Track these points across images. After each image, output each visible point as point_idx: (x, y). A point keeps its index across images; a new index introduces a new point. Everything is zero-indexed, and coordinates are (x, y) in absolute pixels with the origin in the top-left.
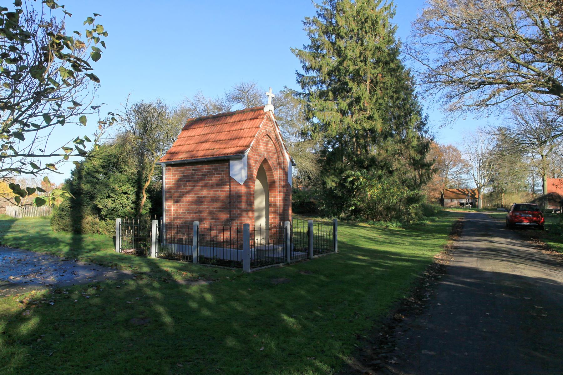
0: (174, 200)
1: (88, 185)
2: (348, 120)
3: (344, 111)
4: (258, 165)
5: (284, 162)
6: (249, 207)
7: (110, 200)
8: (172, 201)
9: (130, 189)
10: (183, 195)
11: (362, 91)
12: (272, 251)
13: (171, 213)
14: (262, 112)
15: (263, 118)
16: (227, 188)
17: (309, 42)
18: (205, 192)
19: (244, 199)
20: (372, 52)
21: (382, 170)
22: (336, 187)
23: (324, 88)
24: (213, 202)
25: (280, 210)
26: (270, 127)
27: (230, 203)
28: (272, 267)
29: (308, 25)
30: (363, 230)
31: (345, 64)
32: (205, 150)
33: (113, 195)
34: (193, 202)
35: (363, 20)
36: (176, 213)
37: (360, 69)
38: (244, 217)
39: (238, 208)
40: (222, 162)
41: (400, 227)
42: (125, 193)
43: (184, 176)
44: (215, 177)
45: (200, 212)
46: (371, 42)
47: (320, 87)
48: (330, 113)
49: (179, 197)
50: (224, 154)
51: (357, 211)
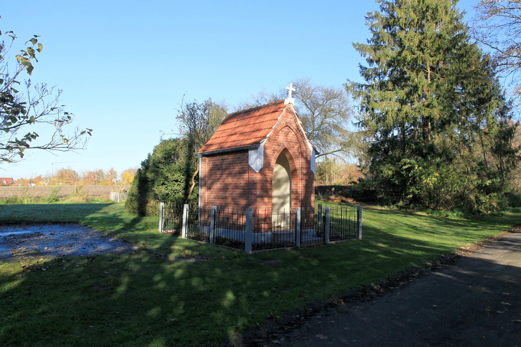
1: (153, 174)
2: (407, 108)
3: (402, 100)
4: (277, 155)
5: (306, 151)
6: (265, 193)
7: (164, 186)
9: (181, 177)
10: (214, 182)
11: (422, 80)
12: (288, 236)
13: (205, 198)
14: (282, 105)
15: (282, 111)
16: (246, 176)
17: (371, 36)
18: (229, 180)
19: (259, 186)
20: (432, 40)
21: (441, 158)
22: (393, 175)
23: (387, 78)
26: (291, 118)
27: (248, 189)
28: (277, 250)
29: (371, 20)
30: (416, 219)
31: (403, 54)
32: (232, 142)
33: (166, 182)
34: (222, 189)
35: (424, 9)
36: (209, 198)
37: (417, 57)
40: (241, 152)
41: (461, 216)
42: (177, 181)
43: (216, 165)
44: (238, 166)
45: (225, 198)
46: (433, 29)
47: (381, 79)
48: (389, 104)
49: (211, 184)
50: (245, 145)
51: (416, 199)
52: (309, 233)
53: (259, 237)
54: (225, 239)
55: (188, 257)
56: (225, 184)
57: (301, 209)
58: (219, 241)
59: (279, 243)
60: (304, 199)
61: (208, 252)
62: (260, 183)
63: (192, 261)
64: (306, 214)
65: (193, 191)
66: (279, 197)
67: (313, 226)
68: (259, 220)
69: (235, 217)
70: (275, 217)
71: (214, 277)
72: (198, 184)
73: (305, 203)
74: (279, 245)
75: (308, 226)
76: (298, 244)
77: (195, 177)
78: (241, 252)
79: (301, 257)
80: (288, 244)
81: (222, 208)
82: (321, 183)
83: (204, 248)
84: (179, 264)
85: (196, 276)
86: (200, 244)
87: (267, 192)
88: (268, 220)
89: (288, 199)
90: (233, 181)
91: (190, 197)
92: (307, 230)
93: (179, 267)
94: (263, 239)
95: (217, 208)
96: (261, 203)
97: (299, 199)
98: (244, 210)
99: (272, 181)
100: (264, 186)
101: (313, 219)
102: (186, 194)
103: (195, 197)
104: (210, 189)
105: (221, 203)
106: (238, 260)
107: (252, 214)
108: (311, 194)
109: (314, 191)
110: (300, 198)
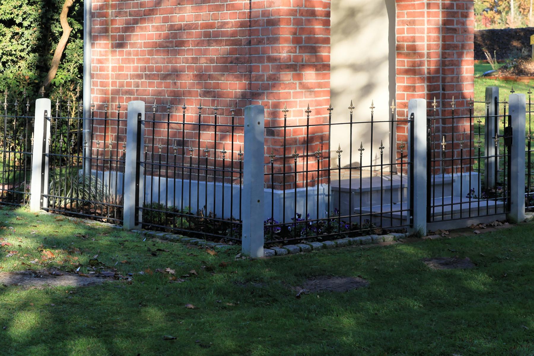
0: (113, 38)
6: (305, 56)
8: (109, 42)
10: (136, 22)
19: (285, 31)
24: (209, 43)
25: (428, 65)
27: (249, 43)
28: (350, 244)
34: (160, 45)
36: (118, 76)
38: (286, 86)
39: (271, 59)
42: (9, 23)
45: (175, 74)
52: (457, 185)
53: (289, 203)
54: (174, 213)
55: (54, 272)
56: (171, 27)
57: (429, 105)
58: (153, 218)
59: (355, 221)
60: (437, 71)
61: (120, 256)
62: (288, 22)
63: (68, 282)
64: (444, 121)
65: (64, 56)
66: (355, 68)
67: (471, 161)
68: (285, 145)
69: (207, 137)
70: (339, 137)
71: (141, 336)
72: (81, 32)
73: (442, 85)
74: (355, 227)
75: (453, 162)
76: (421, 223)
77: (71, 9)
78: (228, 253)
79: (432, 266)
80: (386, 226)
81: (164, 109)
82: (493, 21)
83: (105, 241)
84: (24, 294)
85: (80, 332)
86: (91, 229)
87: (314, 50)
88: (316, 143)
89: (384, 73)
90: (197, 17)
91: (56, 75)
92: (448, 176)
93: (24, 306)
94: (301, 210)
95: (148, 109)
96: (292, 86)
97: (420, 73)
98: (238, 112)
99: (328, 14)
100: (302, 30)
101: (471, 137)
102: (42, 67)
103: (71, 76)
104: (121, 45)
105: (160, 93)
106: (219, 278)
107: (262, 125)
108: (460, 55)
109: (471, 43)
110: (425, 68)
